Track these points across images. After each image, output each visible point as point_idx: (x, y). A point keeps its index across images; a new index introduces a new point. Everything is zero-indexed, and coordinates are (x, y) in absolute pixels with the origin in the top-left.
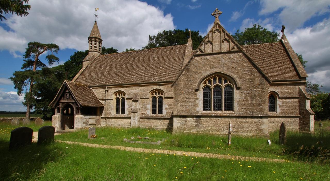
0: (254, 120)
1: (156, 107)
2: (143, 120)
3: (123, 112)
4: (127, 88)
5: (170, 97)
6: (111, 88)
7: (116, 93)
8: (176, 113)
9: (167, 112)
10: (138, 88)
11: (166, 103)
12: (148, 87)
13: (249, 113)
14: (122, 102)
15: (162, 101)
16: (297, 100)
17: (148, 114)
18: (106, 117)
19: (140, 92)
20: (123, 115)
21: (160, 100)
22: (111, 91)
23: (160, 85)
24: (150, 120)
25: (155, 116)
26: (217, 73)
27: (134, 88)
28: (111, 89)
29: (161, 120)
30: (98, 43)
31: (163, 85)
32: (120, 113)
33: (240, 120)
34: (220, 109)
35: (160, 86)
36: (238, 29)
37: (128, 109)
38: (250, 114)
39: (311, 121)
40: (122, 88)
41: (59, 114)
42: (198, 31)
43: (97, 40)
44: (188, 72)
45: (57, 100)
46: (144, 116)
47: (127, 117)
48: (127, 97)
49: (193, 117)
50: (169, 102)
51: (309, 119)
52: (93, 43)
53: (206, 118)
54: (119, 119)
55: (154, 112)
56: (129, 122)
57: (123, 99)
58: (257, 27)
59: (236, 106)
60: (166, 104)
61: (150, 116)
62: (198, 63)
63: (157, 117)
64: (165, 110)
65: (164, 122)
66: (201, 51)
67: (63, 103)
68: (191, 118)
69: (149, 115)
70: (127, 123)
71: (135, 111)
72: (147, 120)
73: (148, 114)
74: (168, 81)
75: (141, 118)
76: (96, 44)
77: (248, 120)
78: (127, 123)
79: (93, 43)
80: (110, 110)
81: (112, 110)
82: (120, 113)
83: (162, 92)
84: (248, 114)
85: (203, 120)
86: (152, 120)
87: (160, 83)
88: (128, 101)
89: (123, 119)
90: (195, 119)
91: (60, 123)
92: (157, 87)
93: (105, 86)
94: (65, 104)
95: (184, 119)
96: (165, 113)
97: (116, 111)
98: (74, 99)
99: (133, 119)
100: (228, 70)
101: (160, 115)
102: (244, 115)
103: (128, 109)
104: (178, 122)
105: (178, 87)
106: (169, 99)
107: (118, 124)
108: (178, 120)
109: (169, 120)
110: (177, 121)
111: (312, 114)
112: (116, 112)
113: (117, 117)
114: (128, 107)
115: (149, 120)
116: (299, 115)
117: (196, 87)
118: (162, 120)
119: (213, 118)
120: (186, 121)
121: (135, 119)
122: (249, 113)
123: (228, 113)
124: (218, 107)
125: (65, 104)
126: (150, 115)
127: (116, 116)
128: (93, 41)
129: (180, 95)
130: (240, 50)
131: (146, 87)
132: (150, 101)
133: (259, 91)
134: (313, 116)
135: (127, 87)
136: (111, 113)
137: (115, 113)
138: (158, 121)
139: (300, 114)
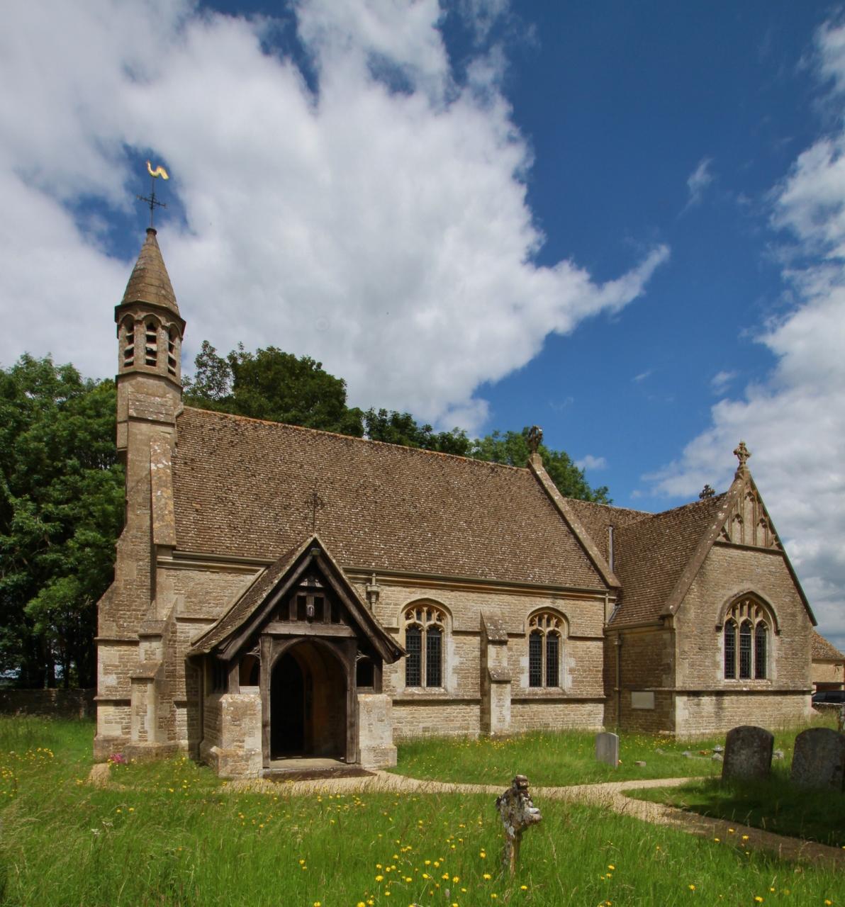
1: (540, 664)
3: (435, 680)
4: (452, 591)
5: (581, 635)
6: (390, 586)
7: (416, 607)
8: (681, 685)
9: (573, 681)
10: (490, 596)
11: (571, 655)
12: (523, 598)
14: (428, 643)
15: (556, 648)
16: (102, 634)
17: (521, 686)
19: (497, 611)
20: (435, 690)
21: (551, 643)
22: (388, 597)
23: (555, 596)
25: (542, 694)
26: (752, 593)
27: (479, 595)
28: (387, 588)
29: (559, 706)
30: (163, 335)
31: (563, 597)
32: (424, 683)
33: (779, 698)
34: (733, 677)
35: (557, 598)
36: (497, 430)
37: (457, 670)
40: (434, 591)
41: (256, 689)
43: (163, 320)
44: (702, 581)
45: (257, 623)
47: (455, 697)
48: (448, 625)
49: (710, 693)
50: (578, 650)
52: (141, 332)
53: (733, 697)
54: (423, 708)
55: (535, 681)
56: (460, 715)
57: (435, 630)
59: (772, 668)
60: (570, 657)
61: (529, 694)
62: (719, 562)
63: (549, 697)
64: (569, 676)
65: (566, 712)
66: (726, 536)
67: (278, 638)
68: (707, 696)
69: (525, 691)
70: (453, 720)
71: (501, 678)
72: (520, 706)
73: (521, 686)
74: (577, 587)
76: (151, 339)
78: (453, 720)
79: (141, 332)
81: (396, 672)
83: (441, 610)
84: (788, 686)
85: (727, 700)
86: (535, 707)
87: (557, 591)
88: (457, 642)
89: (440, 707)
90: (714, 698)
91: (264, 733)
92: (546, 603)
93: (369, 573)
94: (295, 641)
95: (696, 700)
96: (451, 683)
98: (351, 621)
99: (497, 706)
100: (763, 588)
102: (783, 689)
103: (457, 670)
104: (684, 709)
105: (684, 616)
106: (578, 643)
107: (421, 725)
110: (683, 706)
112: (407, 679)
113: (416, 698)
114: (458, 664)
115: (525, 706)
118: (561, 706)
119: (743, 696)
120: (698, 705)
121: (503, 706)
123: (760, 684)
124: (745, 674)
125: (295, 641)
127: (413, 694)
128: (139, 322)
129: (687, 637)
130: (728, 542)
131: (516, 597)
132: (524, 645)
135: (453, 589)
138: (550, 707)
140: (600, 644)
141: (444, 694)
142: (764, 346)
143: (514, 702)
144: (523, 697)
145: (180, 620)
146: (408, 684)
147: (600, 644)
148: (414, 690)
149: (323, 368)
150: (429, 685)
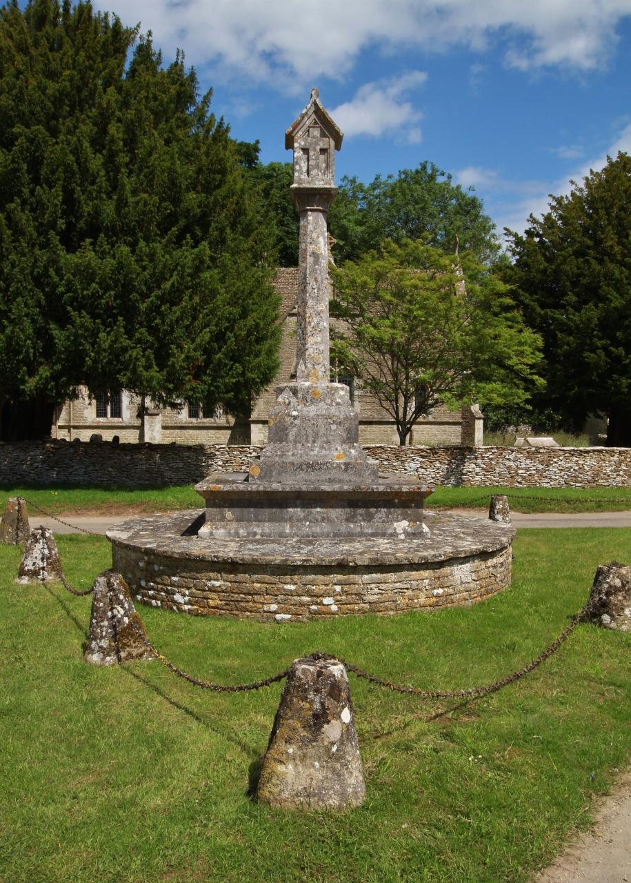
0: (383, 427)
2: (168, 432)
13: (376, 416)
18: (72, 424)
20: (116, 420)
24: (184, 432)
32: (109, 415)
34: (105, 415)
38: (377, 418)
39: (476, 430)
42: (258, 142)
46: (170, 423)
51: (471, 431)
58: (429, 171)
61: (186, 423)
63: (202, 425)
75: (164, 428)
77: (375, 428)
80: (80, 409)
82: (109, 415)
86: (191, 432)
97: (97, 410)
101: (208, 419)
108: (259, 429)
109: (229, 432)
111: (479, 419)
112: (97, 413)
113: (100, 424)
116: (461, 421)
117: (292, 371)
118: (213, 432)
122: (376, 416)
126: (184, 420)
127: (99, 422)
133: (151, 592)
134: (482, 421)
136: (85, 415)
137: (95, 416)
139: (463, 418)
140: (459, 429)
141: (120, 422)
142: (551, 69)
143: (164, 428)
144: (181, 425)
145: (361, 423)
146: (98, 416)
147: (459, 429)
148: (102, 420)
149: (358, 181)
150: (112, 416)
